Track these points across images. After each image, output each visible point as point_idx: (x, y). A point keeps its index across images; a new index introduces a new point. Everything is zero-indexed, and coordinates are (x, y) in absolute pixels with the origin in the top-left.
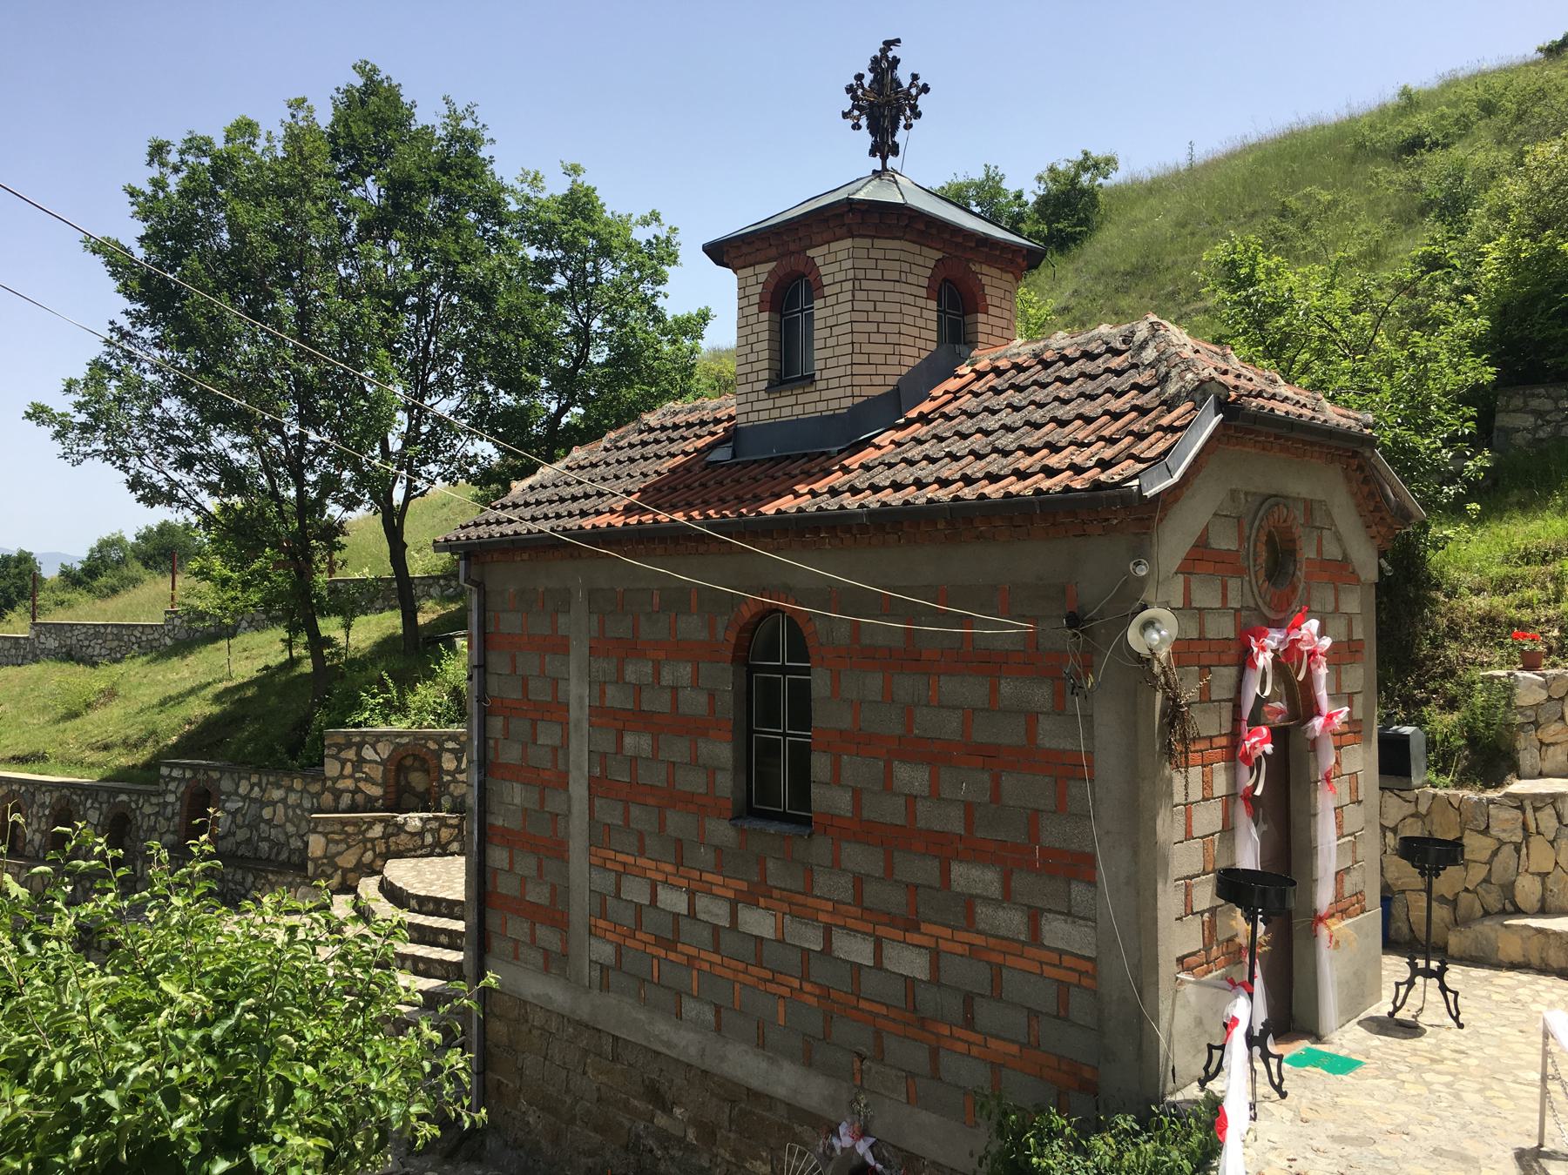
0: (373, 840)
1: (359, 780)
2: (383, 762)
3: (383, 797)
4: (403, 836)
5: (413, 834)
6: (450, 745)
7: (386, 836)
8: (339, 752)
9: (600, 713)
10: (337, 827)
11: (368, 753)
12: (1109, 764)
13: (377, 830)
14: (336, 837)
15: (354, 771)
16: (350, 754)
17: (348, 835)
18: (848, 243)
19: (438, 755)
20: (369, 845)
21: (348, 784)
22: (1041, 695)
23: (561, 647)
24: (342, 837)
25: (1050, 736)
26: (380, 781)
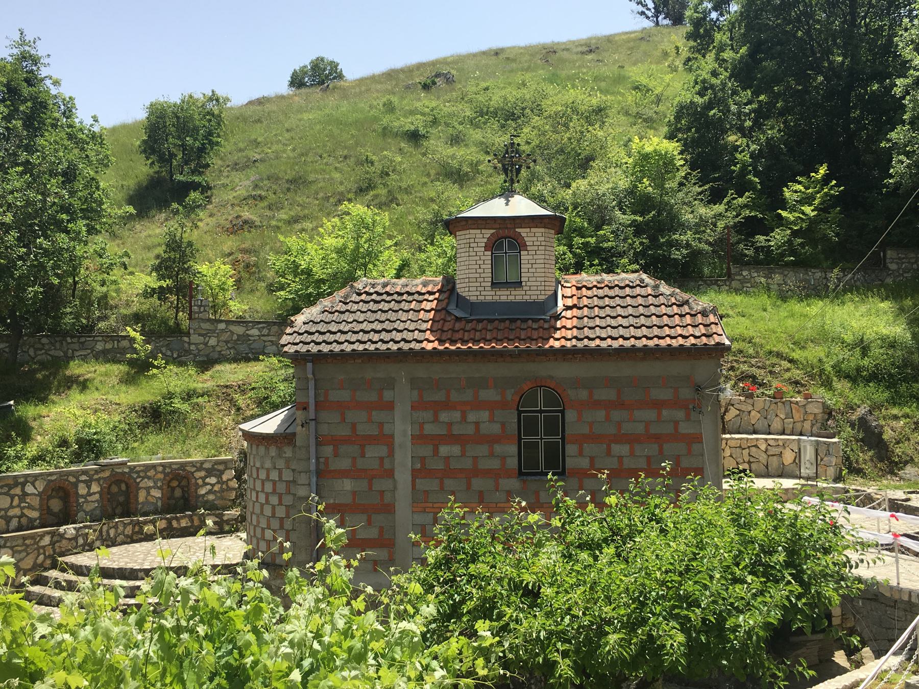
0: (44, 547)
1: (24, 507)
2: (40, 494)
3: (40, 518)
4: (64, 542)
5: (70, 539)
6: (84, 478)
7: (52, 544)
8: (10, 490)
9: (419, 438)
10: (20, 542)
11: (29, 489)
12: (707, 436)
13: (47, 540)
14: (19, 548)
15: (20, 502)
16: (18, 491)
17: (27, 546)
18: (543, 230)
19: (75, 485)
20: (41, 551)
21: (17, 511)
22: (680, 414)
23: (390, 406)
24: (23, 548)
25: (684, 428)
26: (38, 507)
